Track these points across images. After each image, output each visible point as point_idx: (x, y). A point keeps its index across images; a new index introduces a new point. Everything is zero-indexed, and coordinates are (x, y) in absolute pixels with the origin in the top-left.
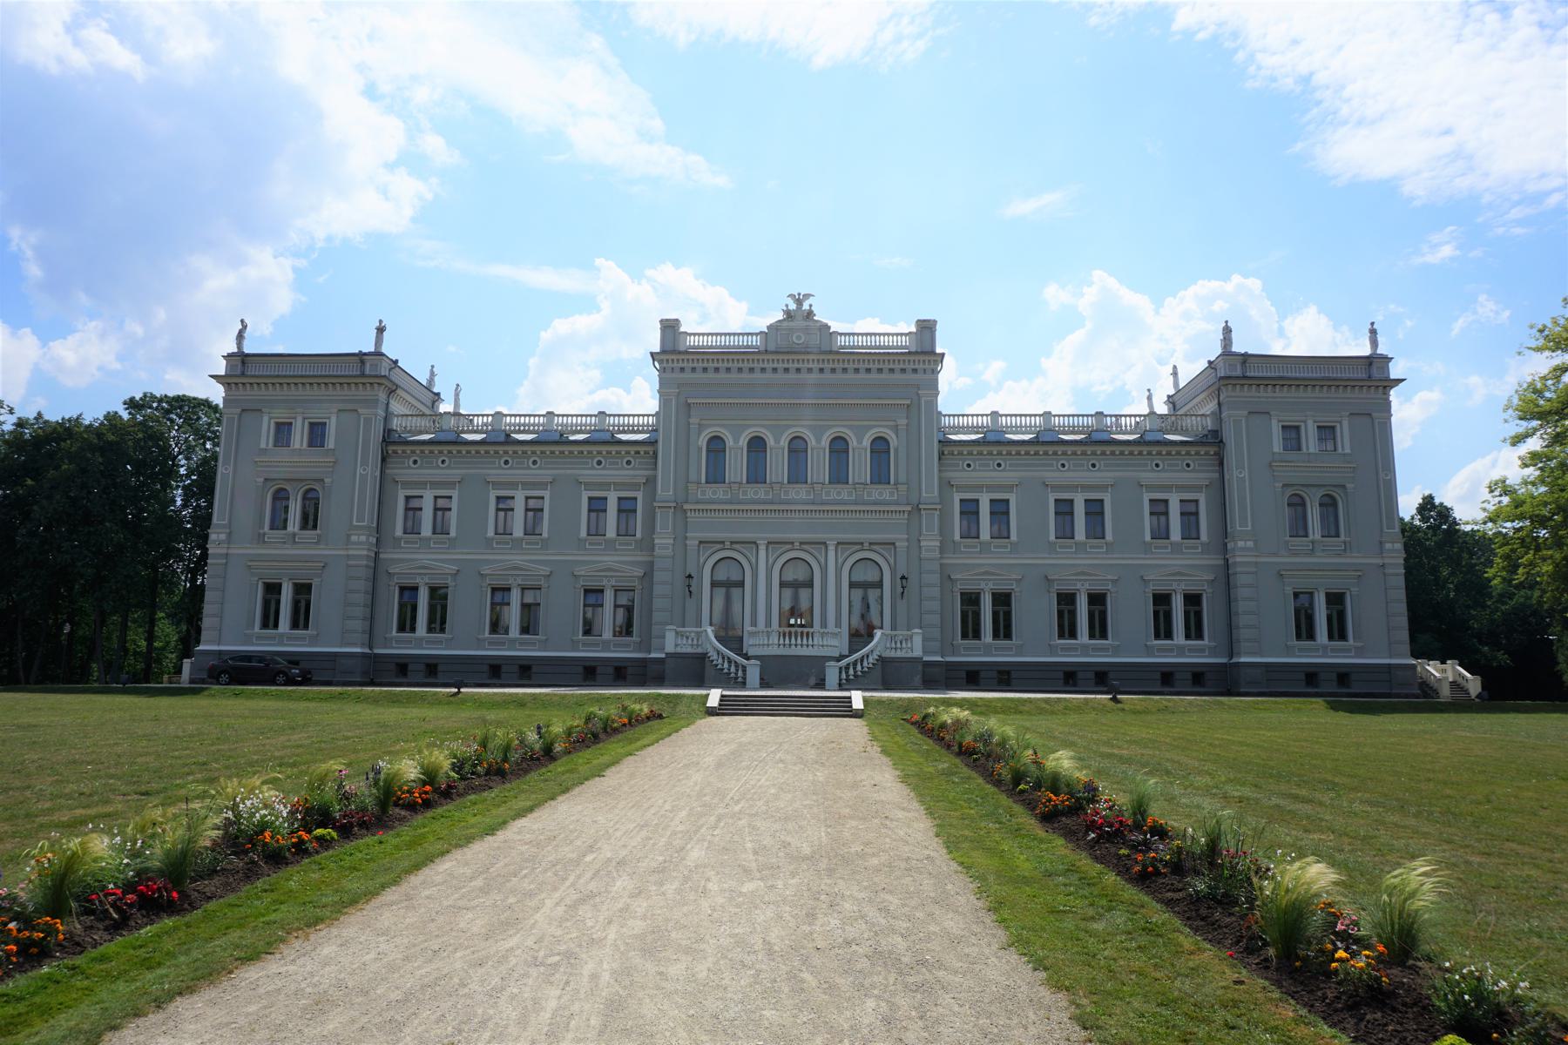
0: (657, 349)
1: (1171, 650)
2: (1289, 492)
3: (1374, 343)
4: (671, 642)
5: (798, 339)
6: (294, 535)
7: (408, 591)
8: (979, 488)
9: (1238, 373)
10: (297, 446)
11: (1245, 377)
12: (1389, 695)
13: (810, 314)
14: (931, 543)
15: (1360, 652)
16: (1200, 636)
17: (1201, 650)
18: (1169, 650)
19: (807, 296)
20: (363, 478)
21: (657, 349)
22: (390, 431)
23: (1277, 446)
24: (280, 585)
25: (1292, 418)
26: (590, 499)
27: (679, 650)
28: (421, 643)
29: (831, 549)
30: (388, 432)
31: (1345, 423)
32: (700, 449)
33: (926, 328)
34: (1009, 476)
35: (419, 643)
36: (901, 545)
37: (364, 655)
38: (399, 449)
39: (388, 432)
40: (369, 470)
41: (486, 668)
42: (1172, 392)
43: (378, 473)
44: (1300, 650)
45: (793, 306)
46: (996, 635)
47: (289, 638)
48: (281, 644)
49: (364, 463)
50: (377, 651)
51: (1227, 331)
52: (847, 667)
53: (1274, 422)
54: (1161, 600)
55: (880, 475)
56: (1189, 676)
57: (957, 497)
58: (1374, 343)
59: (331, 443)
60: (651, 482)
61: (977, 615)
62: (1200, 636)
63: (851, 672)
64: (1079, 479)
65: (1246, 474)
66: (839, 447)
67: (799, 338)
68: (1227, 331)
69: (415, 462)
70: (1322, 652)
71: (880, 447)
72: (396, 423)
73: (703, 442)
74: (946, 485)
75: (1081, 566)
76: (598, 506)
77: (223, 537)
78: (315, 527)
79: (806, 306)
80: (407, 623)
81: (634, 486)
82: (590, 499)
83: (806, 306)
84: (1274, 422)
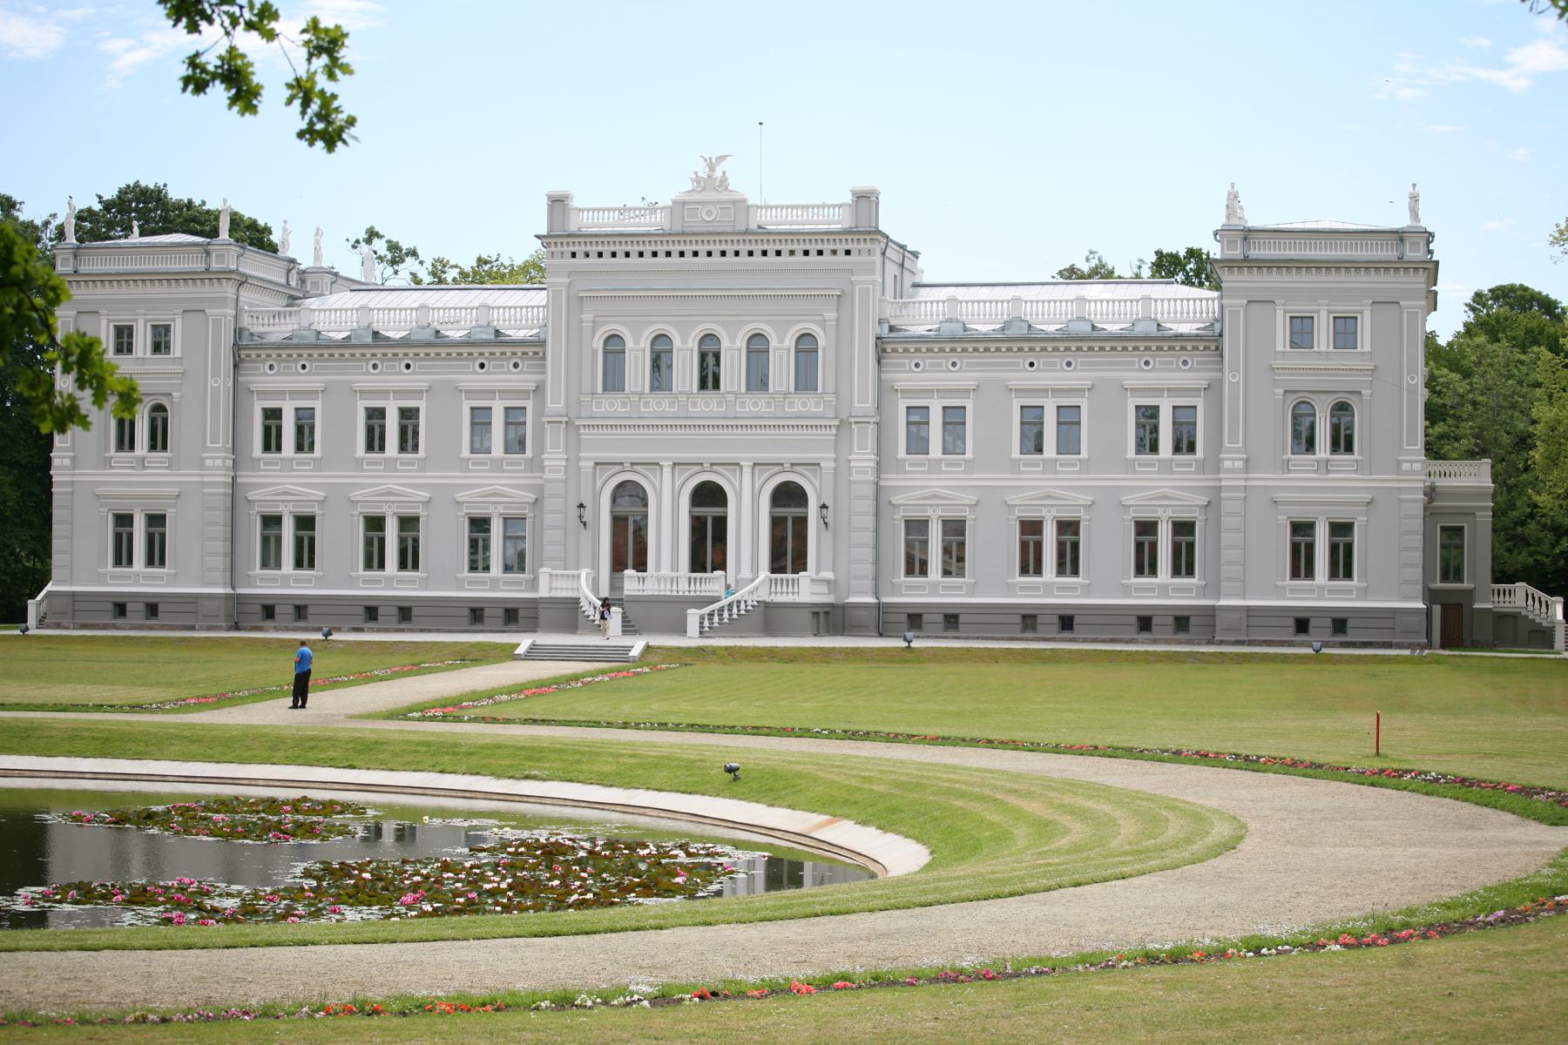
0: (1443, 340)
1: (1152, 590)
2: (1292, 400)
3: (1414, 213)
4: (549, 585)
5: (708, 218)
6: (144, 458)
7: (916, 527)
8: (929, 392)
9: (1237, 253)
10: (140, 355)
11: (1246, 259)
12: (1389, 645)
13: (724, 179)
14: (863, 460)
15: (1364, 593)
16: (1190, 572)
17: (1188, 590)
18: (1149, 589)
19: (722, 158)
20: (215, 390)
21: (544, 232)
22: (241, 330)
23: (1281, 341)
24: (131, 517)
25: (1302, 308)
26: (472, 409)
27: (555, 594)
28: (287, 582)
29: (747, 472)
30: (239, 332)
31: (1367, 314)
32: (594, 352)
33: (865, 200)
34: (964, 377)
35: (286, 581)
36: (828, 465)
37: (227, 596)
38: (253, 354)
39: (239, 332)
40: (220, 382)
41: (361, 611)
42: (576, 203)
43: (230, 384)
44: (1292, 591)
45: (703, 174)
46: (1334, 574)
47: (296, 581)
48: (137, 584)
49: (216, 374)
50: (240, 591)
51: (1233, 197)
52: (711, 615)
53: (1280, 313)
54: (1146, 529)
55: (806, 380)
56: (1170, 620)
57: (902, 405)
58: (1414, 213)
59: (1365, 342)
60: (539, 389)
61: (1039, 546)
62: (1190, 572)
63: (726, 614)
64: (1052, 379)
65: (1240, 377)
66: (757, 346)
67: (709, 213)
68: (1233, 197)
69: (271, 367)
70: (1321, 593)
71: (806, 346)
72: (246, 322)
73: (598, 344)
74: (883, 392)
75: (1050, 487)
76: (480, 420)
77: (67, 462)
78: (165, 448)
79: (718, 174)
80: (270, 557)
81: (524, 394)
82: (472, 409)
83: (718, 174)
84: (1280, 313)
